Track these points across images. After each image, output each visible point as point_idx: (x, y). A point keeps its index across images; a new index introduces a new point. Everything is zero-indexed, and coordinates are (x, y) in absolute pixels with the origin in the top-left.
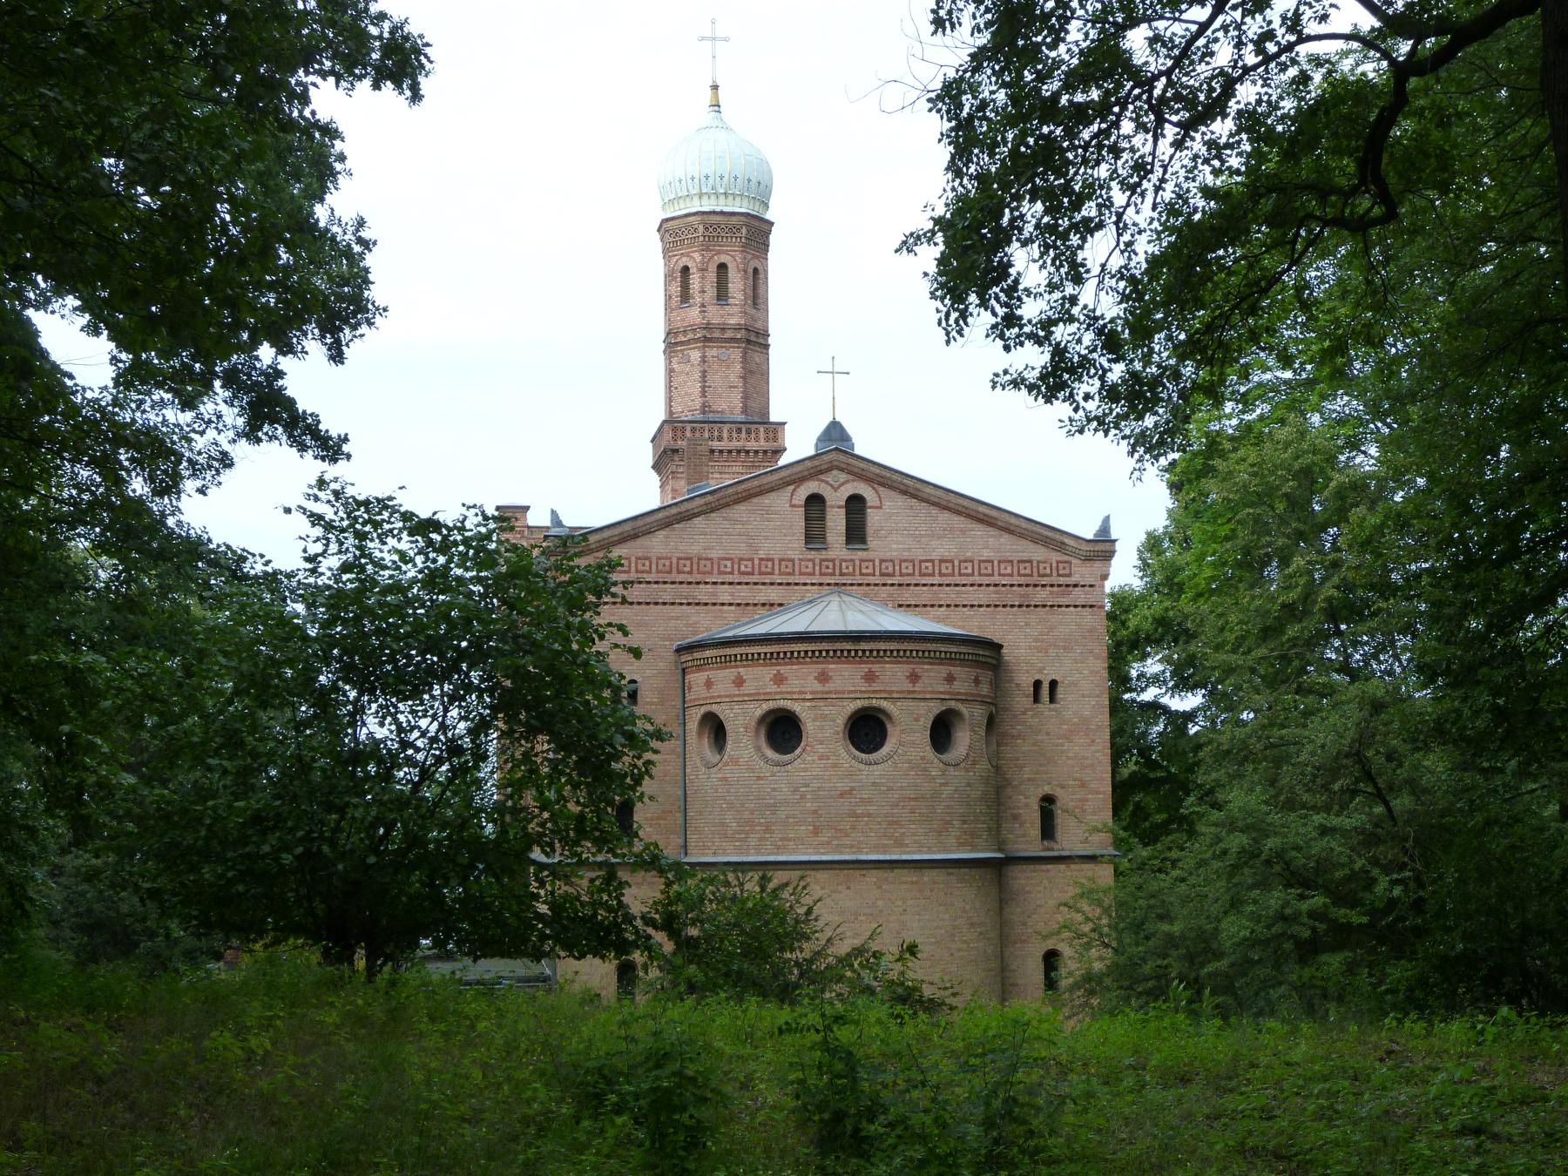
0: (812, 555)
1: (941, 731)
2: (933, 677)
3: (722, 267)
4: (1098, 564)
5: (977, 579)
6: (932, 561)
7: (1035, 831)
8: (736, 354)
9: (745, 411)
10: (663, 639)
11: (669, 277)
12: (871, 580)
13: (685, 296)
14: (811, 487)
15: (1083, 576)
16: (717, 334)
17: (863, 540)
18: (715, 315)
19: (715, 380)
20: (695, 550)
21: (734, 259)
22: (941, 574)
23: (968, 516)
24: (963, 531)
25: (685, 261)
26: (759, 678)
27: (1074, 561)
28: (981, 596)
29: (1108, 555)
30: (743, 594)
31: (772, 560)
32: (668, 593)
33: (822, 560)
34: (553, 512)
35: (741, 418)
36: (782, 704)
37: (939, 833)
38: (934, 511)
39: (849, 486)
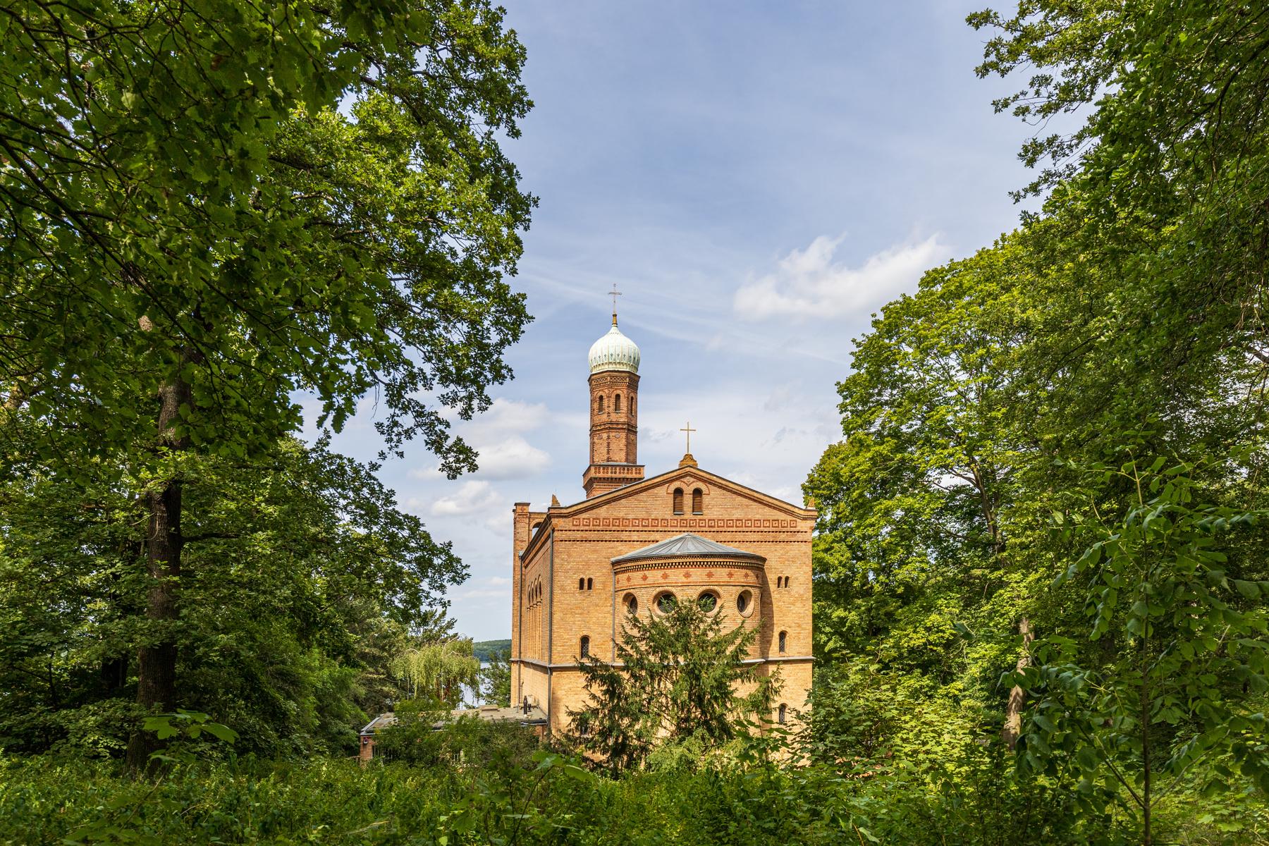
1: (742, 601)
8: (623, 435)
9: (627, 460)
13: (601, 409)
17: (700, 509)
18: (614, 417)
19: (613, 446)
20: (621, 515)
21: (623, 393)
26: (655, 576)
30: (644, 536)
32: (607, 536)
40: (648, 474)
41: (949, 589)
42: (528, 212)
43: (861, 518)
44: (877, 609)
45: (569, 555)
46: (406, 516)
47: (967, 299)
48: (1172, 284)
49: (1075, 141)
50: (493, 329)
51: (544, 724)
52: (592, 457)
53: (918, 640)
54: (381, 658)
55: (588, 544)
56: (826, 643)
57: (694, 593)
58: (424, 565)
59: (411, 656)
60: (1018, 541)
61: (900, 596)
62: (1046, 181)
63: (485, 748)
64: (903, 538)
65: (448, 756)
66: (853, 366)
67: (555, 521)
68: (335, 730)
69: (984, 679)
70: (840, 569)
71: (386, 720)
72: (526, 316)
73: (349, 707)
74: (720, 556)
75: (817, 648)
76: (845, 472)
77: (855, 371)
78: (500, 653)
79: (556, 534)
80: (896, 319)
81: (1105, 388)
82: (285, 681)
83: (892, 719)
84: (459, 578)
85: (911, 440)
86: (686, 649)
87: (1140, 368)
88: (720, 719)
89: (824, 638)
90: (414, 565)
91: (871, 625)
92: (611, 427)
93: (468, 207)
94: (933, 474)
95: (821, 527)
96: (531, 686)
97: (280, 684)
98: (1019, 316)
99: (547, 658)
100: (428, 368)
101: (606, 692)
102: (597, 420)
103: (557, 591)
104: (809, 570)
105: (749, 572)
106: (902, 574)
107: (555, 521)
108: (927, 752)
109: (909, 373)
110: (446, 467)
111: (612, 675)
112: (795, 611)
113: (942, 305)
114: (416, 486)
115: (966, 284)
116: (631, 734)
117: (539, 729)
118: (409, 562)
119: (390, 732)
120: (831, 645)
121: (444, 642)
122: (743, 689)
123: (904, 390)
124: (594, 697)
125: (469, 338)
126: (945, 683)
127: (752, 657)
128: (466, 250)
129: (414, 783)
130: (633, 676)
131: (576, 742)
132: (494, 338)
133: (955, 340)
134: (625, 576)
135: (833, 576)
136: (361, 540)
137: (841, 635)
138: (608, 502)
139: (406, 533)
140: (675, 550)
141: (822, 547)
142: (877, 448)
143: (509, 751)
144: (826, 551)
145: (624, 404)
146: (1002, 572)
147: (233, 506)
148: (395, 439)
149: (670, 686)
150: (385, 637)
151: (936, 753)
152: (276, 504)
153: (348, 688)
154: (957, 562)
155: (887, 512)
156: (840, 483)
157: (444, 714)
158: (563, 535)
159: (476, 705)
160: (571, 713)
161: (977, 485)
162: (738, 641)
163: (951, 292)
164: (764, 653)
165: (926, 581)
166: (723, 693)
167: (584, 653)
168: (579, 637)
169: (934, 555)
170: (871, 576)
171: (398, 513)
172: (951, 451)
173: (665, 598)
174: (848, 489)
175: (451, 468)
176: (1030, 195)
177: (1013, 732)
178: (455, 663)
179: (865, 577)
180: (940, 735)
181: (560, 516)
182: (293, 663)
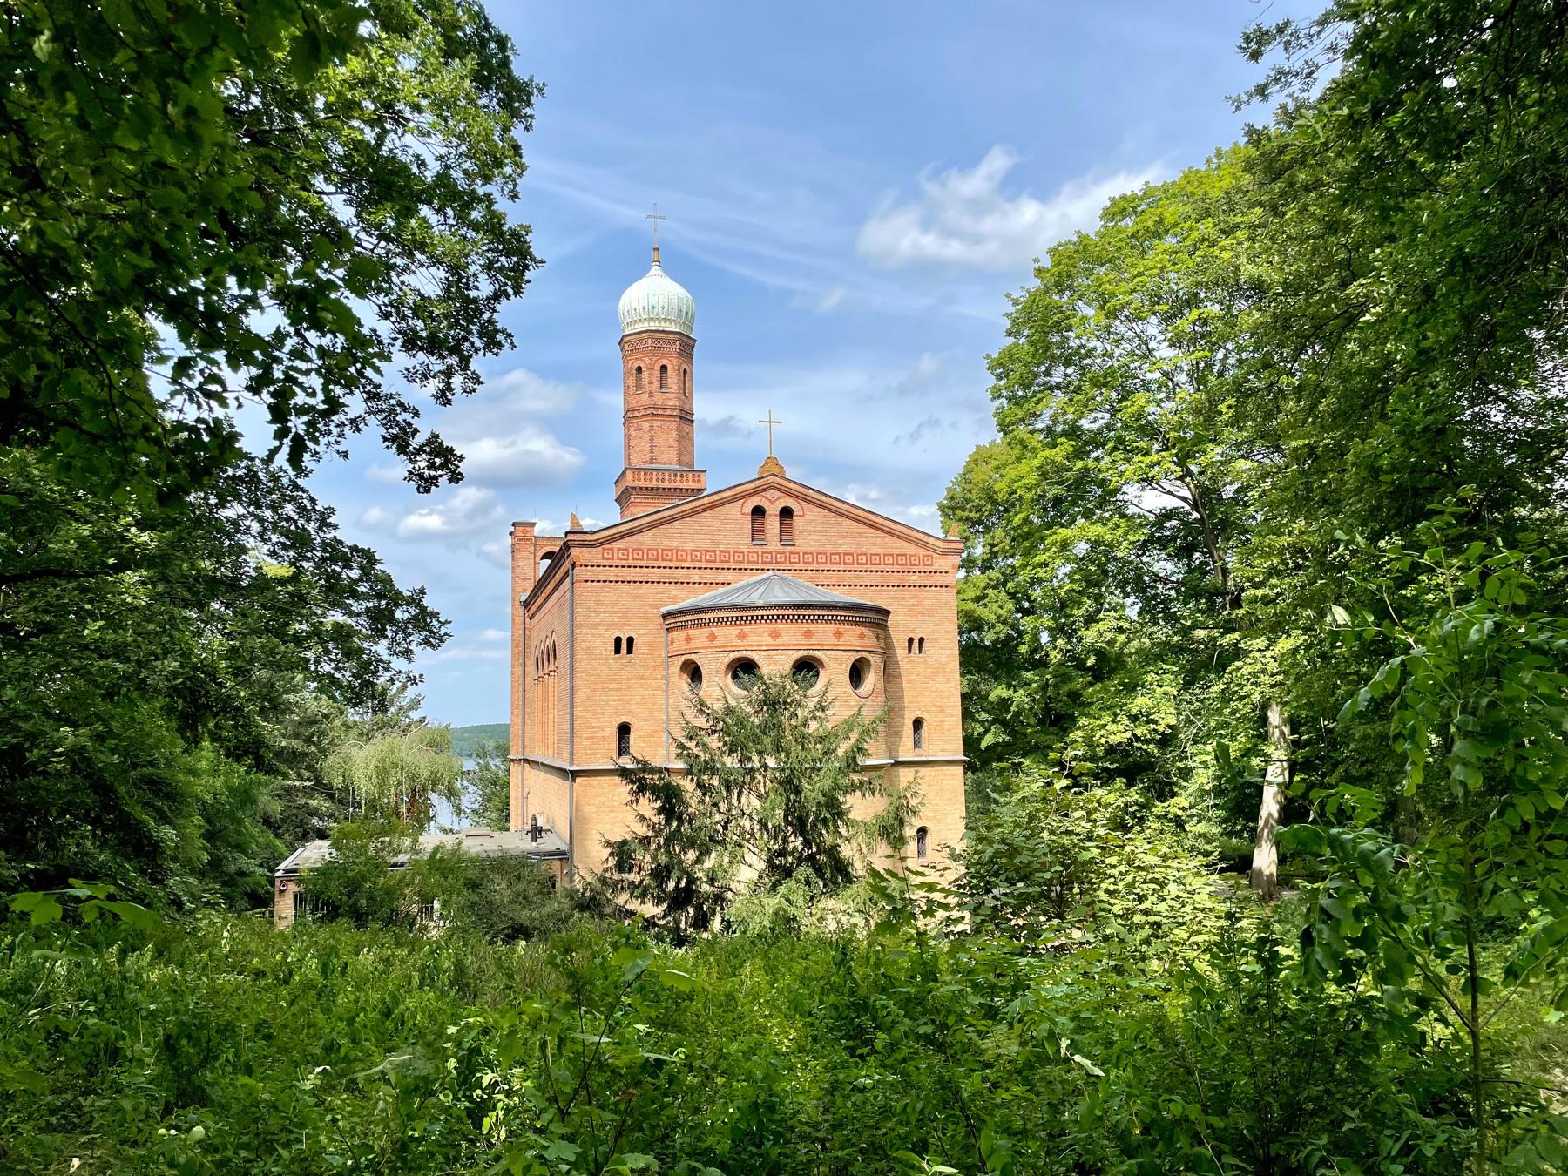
1: (857, 673)
3: (664, 368)
5: (870, 567)
8: (673, 425)
9: (679, 463)
12: (797, 567)
13: (639, 386)
14: (755, 501)
17: (791, 538)
18: (659, 399)
19: (658, 442)
20: (675, 544)
21: (672, 364)
26: (727, 634)
30: (709, 576)
32: (655, 575)
36: (744, 654)
40: (711, 484)
41: (1160, 658)
42: (529, 104)
43: (1027, 553)
44: (1055, 686)
45: (598, 603)
46: (355, 549)
47: (1170, 241)
48: (1462, 248)
49: (1315, 29)
50: (482, 277)
51: (563, 856)
52: (628, 457)
53: (1117, 733)
54: (305, 755)
55: (625, 587)
56: (981, 737)
57: (786, 662)
58: (380, 620)
59: (354, 751)
60: (1260, 593)
61: (1090, 669)
62: (1277, 81)
63: (474, 898)
64: (1090, 584)
65: (415, 909)
66: (1009, 334)
67: (575, 551)
68: (233, 868)
69: (1218, 791)
70: (999, 627)
71: (315, 853)
72: (533, 259)
73: (255, 832)
75: (970, 743)
76: (1001, 487)
77: (1012, 340)
78: (495, 746)
79: (577, 570)
80: (1070, 267)
81: (1374, 374)
82: (156, 793)
83: (1092, 861)
84: (434, 640)
85: (1097, 441)
86: (778, 748)
87: (1424, 358)
88: (833, 852)
89: (979, 729)
90: (363, 620)
91: (1047, 710)
92: (655, 412)
93: (444, 100)
94: (1131, 491)
95: (968, 564)
96: (540, 799)
97: (147, 797)
98: (1249, 270)
99: (566, 756)
100: (385, 329)
101: (660, 811)
103: (580, 655)
104: (953, 628)
105: (865, 630)
106: (1090, 635)
107: (575, 551)
108: (1146, 912)
109: (1090, 345)
110: (416, 475)
111: (668, 786)
112: (935, 686)
113: (1133, 247)
114: (358, 494)
115: (1169, 220)
116: (699, 875)
117: (556, 865)
118: (358, 615)
119: (326, 871)
120: (989, 740)
121: (405, 731)
122: (862, 807)
123: (1082, 368)
124: (642, 819)
125: (447, 290)
126: (1162, 798)
127: (876, 757)
128: (440, 158)
129: (370, 957)
130: (700, 786)
131: (617, 887)
132: (485, 288)
133: (1156, 299)
134: (683, 633)
135: (988, 638)
136: (282, 581)
137: (1004, 723)
138: (654, 525)
139: (355, 574)
140: (756, 598)
141: (971, 594)
142: (1047, 453)
143: (505, 898)
144: (977, 600)
145: (673, 378)
146: (1237, 635)
147: (85, 531)
148: (335, 431)
149: (756, 803)
150: (314, 722)
151: (1158, 914)
152: (152, 528)
153: (255, 802)
154: (1171, 618)
155: (1065, 546)
156: (995, 503)
157: (407, 842)
158: (589, 573)
159: (456, 828)
160: (608, 844)
161: (1195, 507)
162: (854, 735)
163: (1147, 230)
164: (891, 752)
165: (1125, 644)
166: (833, 810)
167: (623, 750)
168: (616, 724)
169: (1137, 608)
170: (1045, 638)
171: (341, 542)
172: (1155, 458)
173: (744, 668)
174: (1006, 511)
175: (421, 477)
176: (1256, 100)
177: (1267, 872)
178: (422, 763)
179: (1036, 638)
180: (1163, 885)
181: (582, 545)
182: (169, 765)
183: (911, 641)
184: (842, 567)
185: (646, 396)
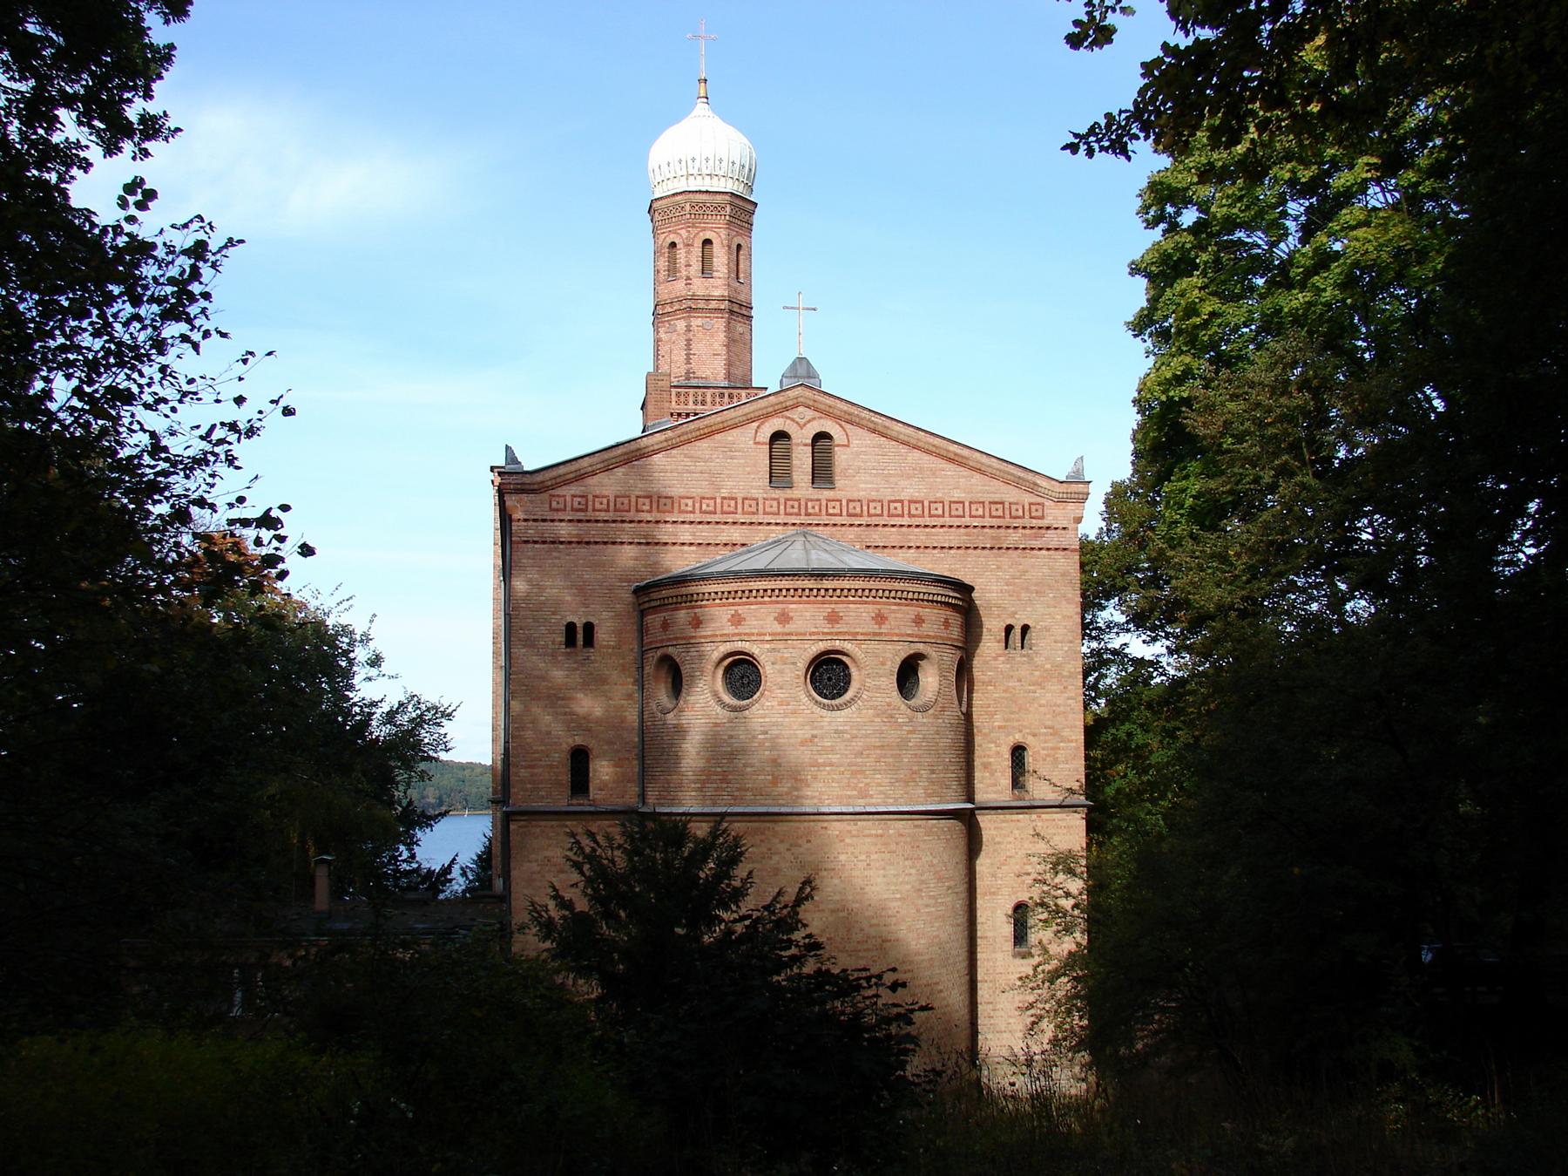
0: (777, 493)
1: (907, 674)
2: (900, 617)
4: (1071, 506)
5: (948, 521)
6: (902, 502)
7: (1006, 780)
8: (719, 324)
9: (728, 376)
10: (621, 580)
11: (657, 253)
12: (838, 520)
13: (672, 270)
14: (776, 424)
15: (1055, 518)
16: (701, 305)
18: (700, 287)
21: (719, 236)
22: (910, 516)
23: (939, 455)
24: (933, 472)
25: (672, 238)
27: (1048, 503)
28: (953, 538)
29: (1083, 498)
31: (735, 499)
33: (787, 500)
34: (507, 448)
35: (725, 383)
36: (739, 646)
37: (906, 783)
38: (903, 449)
39: (815, 423)
74: (857, 574)
92: (692, 307)
102: (667, 292)
183: (1009, 629)
184: (906, 521)
185: (680, 284)
